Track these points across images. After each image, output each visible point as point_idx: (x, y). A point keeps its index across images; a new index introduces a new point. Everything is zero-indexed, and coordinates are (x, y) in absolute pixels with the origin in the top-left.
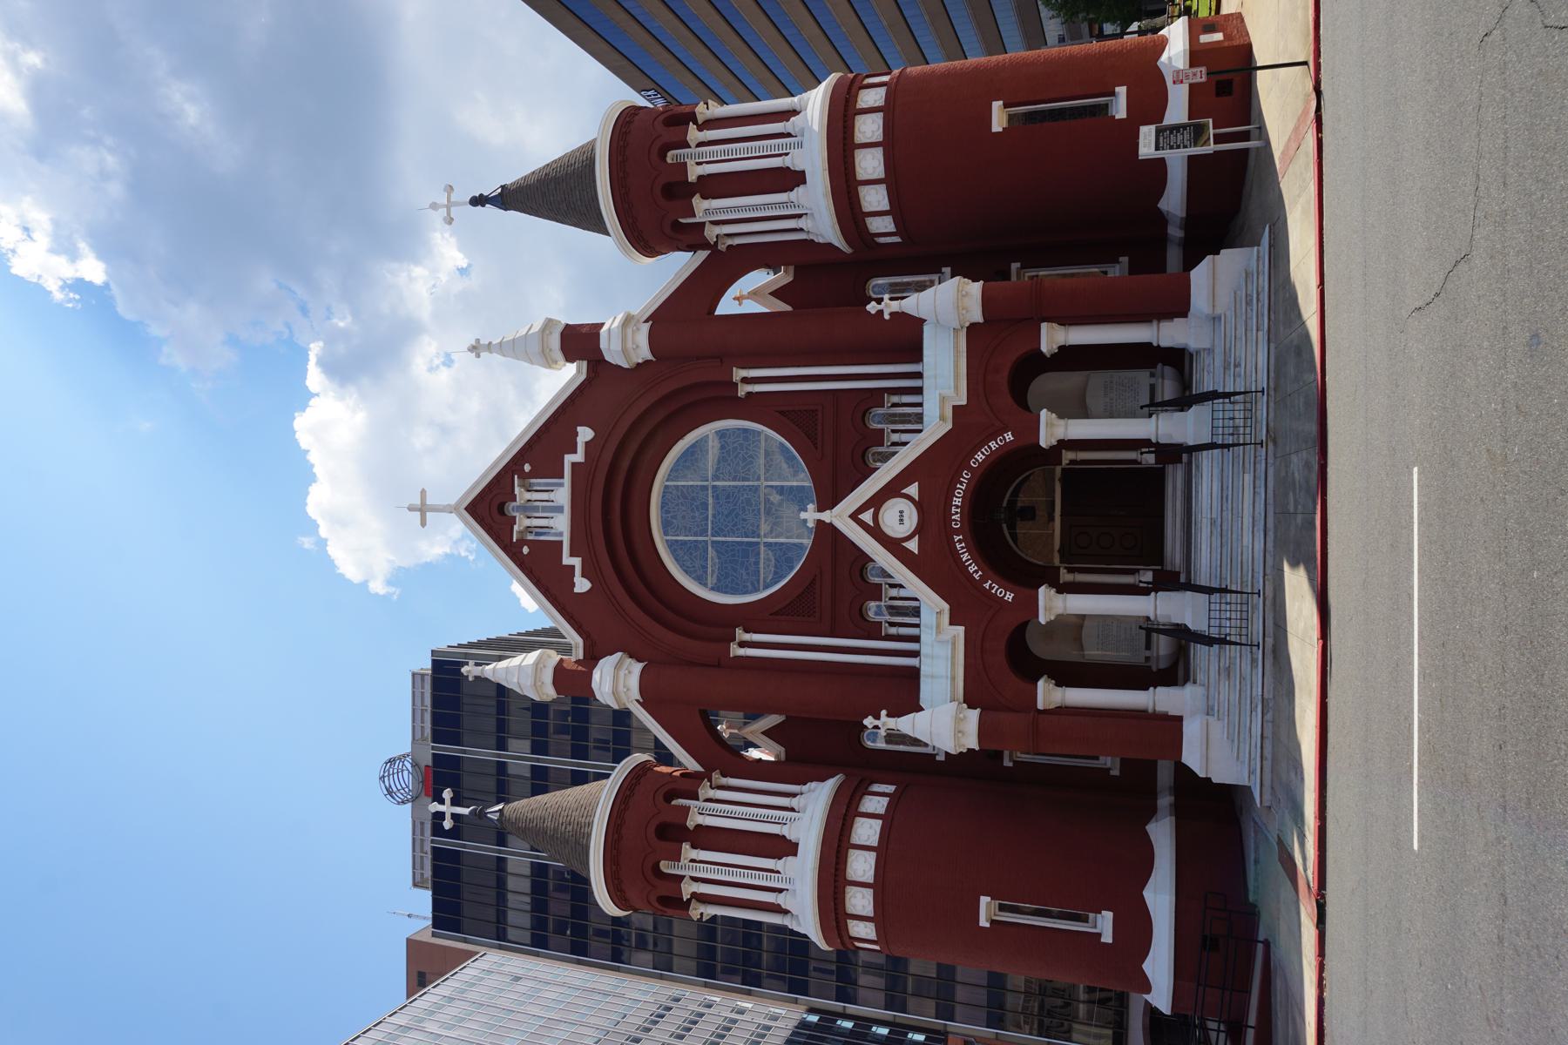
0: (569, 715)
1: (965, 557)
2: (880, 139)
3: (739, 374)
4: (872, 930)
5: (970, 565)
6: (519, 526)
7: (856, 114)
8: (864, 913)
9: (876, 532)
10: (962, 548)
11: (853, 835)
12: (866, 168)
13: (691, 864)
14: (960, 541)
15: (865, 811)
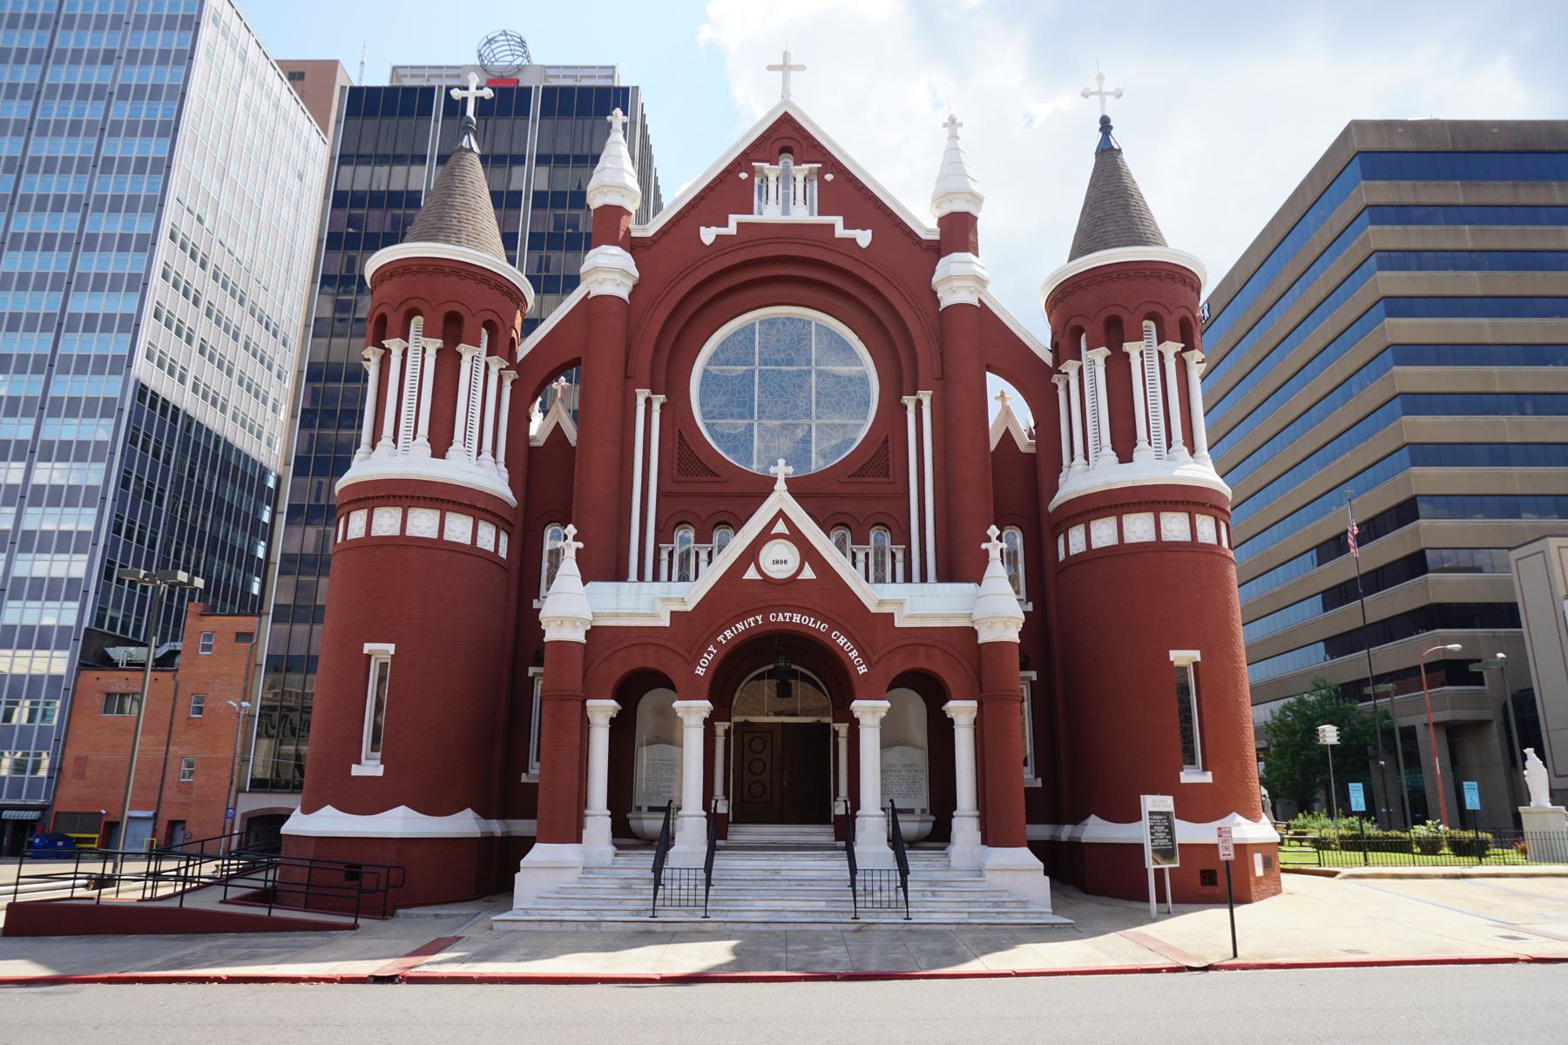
1: (740, 627)
3: (926, 396)
5: (732, 632)
6: (769, 169)
7: (1189, 513)
9: (765, 536)
10: (749, 624)
13: (421, 349)
14: (756, 621)
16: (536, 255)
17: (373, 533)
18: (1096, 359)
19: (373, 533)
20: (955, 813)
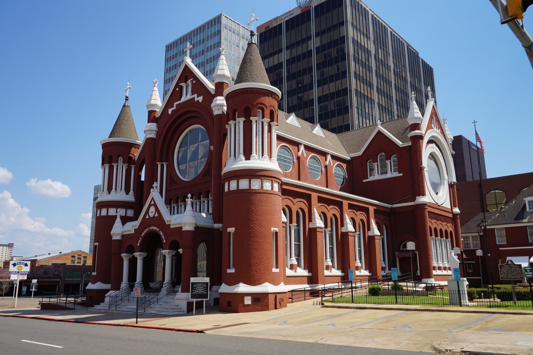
0: (330, 57)
1: (145, 232)
2: (252, 188)
4: (233, 189)
6: (183, 85)
11: (111, 208)
12: (255, 182)
16: (319, 72)
17: (109, 215)
18: (241, 121)
19: (109, 215)
20: (122, 283)
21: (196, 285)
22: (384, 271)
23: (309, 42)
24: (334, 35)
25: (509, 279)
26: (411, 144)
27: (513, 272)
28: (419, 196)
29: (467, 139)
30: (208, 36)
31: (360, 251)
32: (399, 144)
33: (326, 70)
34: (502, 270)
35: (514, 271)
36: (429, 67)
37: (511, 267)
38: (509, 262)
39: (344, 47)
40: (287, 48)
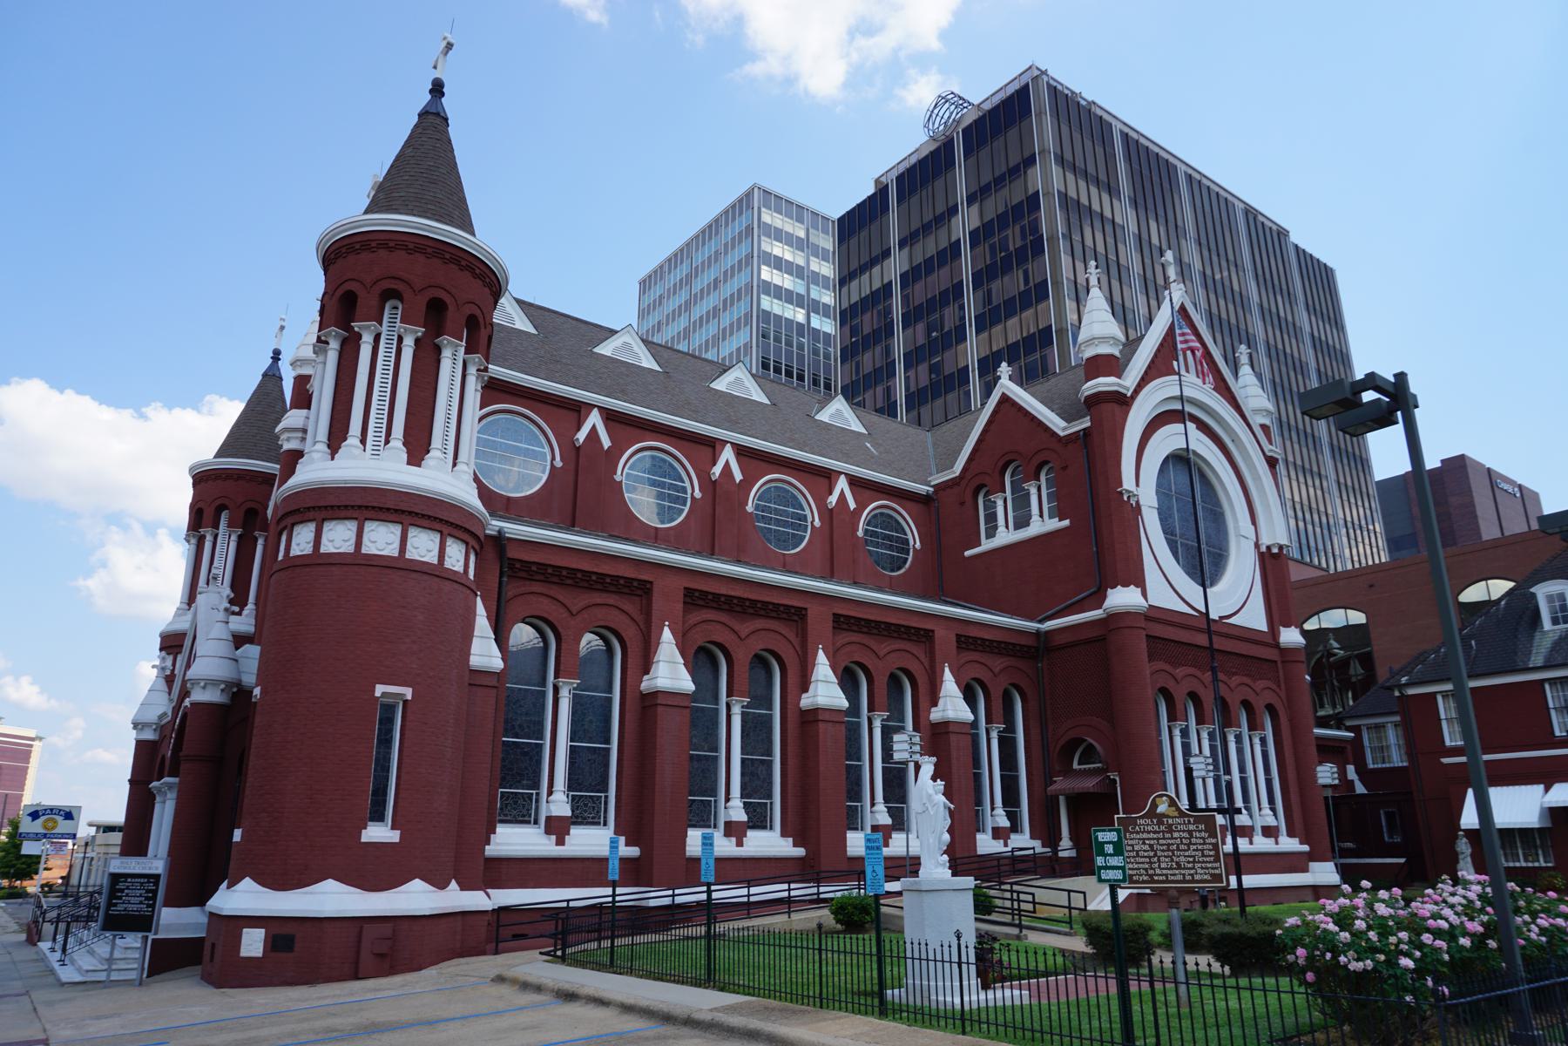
8: (324, 540)
13: (396, 338)
15: (448, 544)
21: (125, 882)
22: (1002, 841)
23: (953, 220)
24: (1013, 194)
25: (1198, 882)
26: (1089, 424)
27: (1178, 849)
28: (1114, 587)
29: (1484, 466)
30: (726, 245)
31: (1269, 783)
32: (1057, 426)
33: (996, 286)
34: (1130, 842)
35: (1182, 847)
36: (1315, 262)
37: (1170, 829)
38: (1164, 803)
39: (1037, 222)
40: (902, 244)
